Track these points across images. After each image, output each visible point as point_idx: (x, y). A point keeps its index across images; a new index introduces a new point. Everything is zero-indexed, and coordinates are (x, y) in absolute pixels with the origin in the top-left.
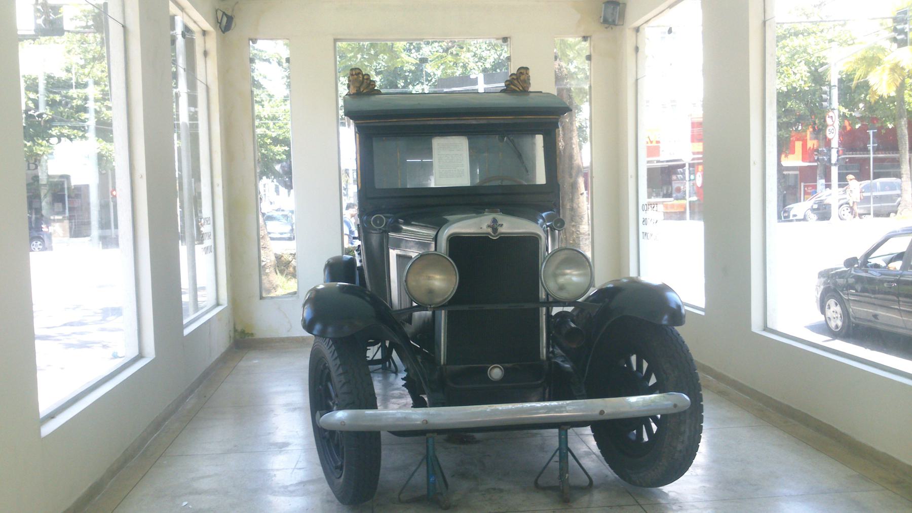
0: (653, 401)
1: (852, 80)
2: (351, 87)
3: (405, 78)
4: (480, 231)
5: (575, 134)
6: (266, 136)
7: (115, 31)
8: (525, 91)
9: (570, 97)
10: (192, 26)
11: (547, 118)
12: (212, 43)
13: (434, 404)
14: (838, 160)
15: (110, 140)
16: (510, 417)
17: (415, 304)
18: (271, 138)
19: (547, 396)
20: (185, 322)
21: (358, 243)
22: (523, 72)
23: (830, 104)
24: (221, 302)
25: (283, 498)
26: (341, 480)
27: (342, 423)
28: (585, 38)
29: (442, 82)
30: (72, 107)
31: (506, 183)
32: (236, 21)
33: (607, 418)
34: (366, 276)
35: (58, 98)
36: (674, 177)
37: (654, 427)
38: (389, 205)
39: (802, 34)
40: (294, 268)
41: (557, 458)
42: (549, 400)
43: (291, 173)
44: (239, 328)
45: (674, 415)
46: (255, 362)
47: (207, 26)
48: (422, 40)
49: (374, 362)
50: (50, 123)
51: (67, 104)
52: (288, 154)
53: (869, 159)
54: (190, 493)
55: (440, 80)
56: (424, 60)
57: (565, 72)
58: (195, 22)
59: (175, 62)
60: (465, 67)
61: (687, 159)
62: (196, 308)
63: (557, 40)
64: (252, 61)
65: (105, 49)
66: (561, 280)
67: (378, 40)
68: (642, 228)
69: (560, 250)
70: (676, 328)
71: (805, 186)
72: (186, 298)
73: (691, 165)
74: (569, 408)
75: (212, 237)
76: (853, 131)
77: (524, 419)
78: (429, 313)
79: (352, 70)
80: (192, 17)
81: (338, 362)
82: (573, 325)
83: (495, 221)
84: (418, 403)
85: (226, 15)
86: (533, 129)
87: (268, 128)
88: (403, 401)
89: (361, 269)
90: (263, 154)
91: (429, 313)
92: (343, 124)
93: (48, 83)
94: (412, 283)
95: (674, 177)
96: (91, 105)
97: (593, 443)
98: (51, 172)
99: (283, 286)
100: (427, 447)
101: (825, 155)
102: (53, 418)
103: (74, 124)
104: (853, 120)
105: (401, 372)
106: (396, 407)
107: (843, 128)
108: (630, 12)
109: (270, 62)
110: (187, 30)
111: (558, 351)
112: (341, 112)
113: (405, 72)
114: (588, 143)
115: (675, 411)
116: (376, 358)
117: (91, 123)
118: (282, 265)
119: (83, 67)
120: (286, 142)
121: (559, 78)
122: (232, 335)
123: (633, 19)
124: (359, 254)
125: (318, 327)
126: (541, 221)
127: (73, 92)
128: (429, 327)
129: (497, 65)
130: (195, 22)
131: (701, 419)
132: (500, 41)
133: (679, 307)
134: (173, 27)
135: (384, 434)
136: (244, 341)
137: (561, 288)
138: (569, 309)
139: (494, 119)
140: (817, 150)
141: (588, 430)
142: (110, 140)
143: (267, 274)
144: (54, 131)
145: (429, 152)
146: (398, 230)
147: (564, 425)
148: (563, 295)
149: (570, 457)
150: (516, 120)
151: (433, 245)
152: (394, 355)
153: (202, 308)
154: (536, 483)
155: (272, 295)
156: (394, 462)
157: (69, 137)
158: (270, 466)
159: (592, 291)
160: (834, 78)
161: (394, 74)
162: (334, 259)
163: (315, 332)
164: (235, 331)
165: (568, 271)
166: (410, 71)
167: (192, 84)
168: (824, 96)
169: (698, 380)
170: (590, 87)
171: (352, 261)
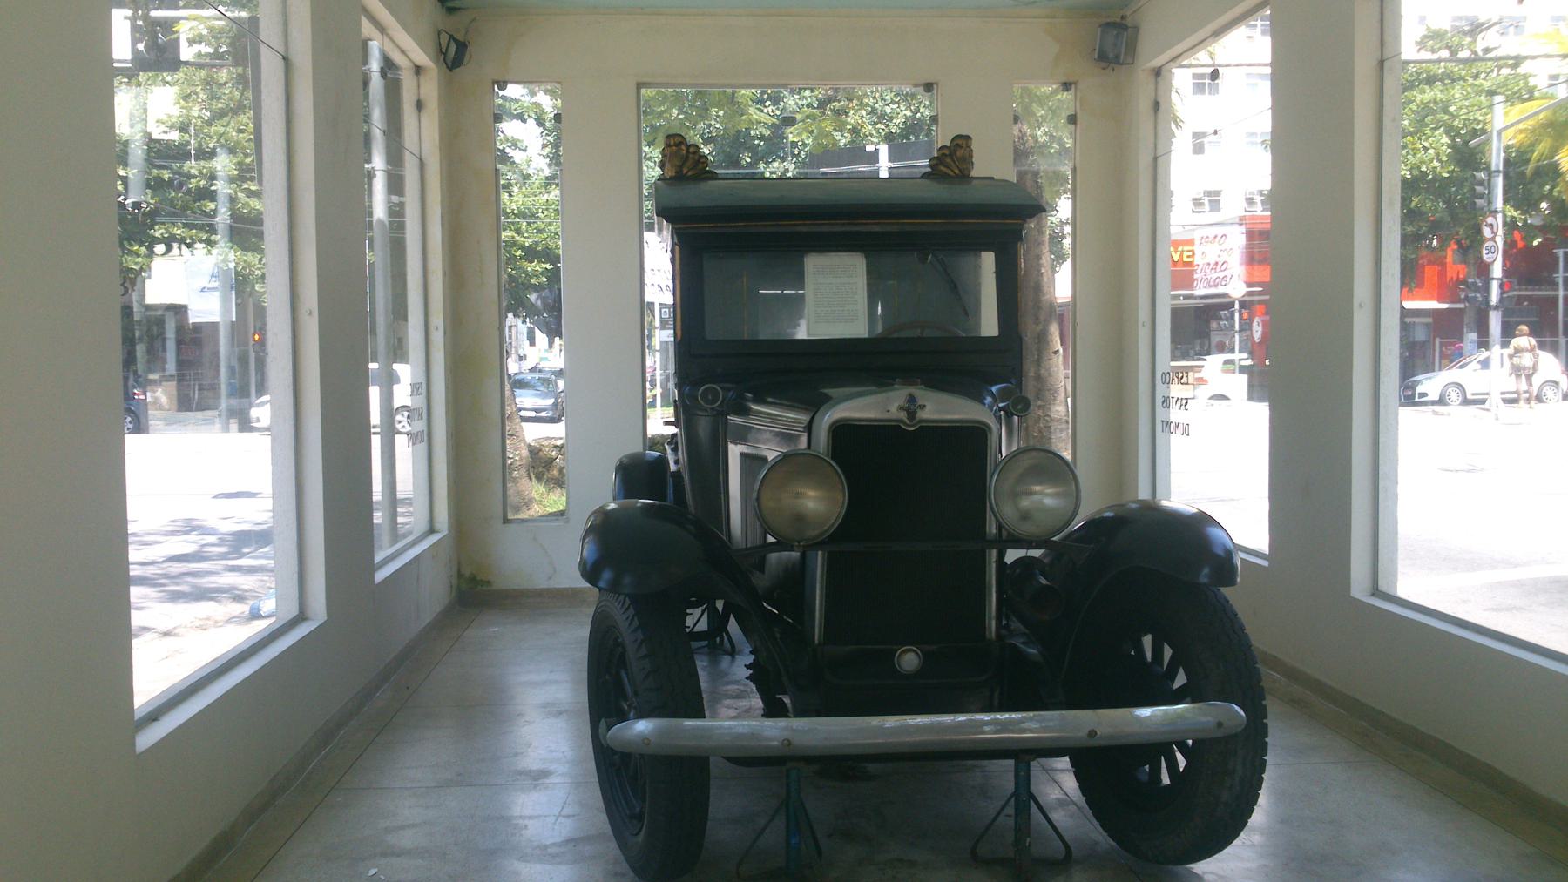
0: (1180, 716)
1: (1528, 161)
2: (668, 165)
3: (753, 150)
4: (886, 416)
5: (1046, 249)
6: (514, 243)
7: (271, 67)
8: (964, 177)
9: (1038, 187)
10: (397, 58)
11: (1005, 223)
12: (431, 88)
13: (801, 713)
14: (1501, 300)
15: (258, 249)
16: (925, 738)
17: (771, 539)
18: (523, 248)
19: (996, 702)
20: (378, 558)
21: (672, 430)
22: (961, 144)
23: (1490, 202)
24: (438, 526)
25: (538, 867)
26: (640, 838)
27: (645, 740)
28: (1066, 86)
29: (817, 159)
30: (189, 191)
31: (928, 333)
32: (471, 49)
33: (1103, 743)
34: (688, 488)
35: (166, 175)
36: (1214, 325)
37: (1182, 762)
38: (725, 367)
39: (1442, 80)
40: (561, 470)
41: (1010, 810)
42: (1001, 709)
43: (560, 310)
44: (467, 572)
45: (1217, 741)
46: (495, 631)
47: (422, 58)
48: (785, 86)
49: (699, 636)
50: (153, 217)
51: (181, 185)
52: (554, 276)
53: (1556, 298)
54: (384, 855)
55: (810, 155)
56: (789, 121)
57: (1031, 142)
58: (403, 52)
59: (367, 119)
60: (855, 131)
61: (1237, 289)
62: (395, 536)
63: (1017, 89)
64: (498, 118)
65: (249, 94)
66: (1025, 503)
67: (712, 85)
68: (1160, 413)
69: (1021, 452)
70: (1224, 590)
71: (1442, 345)
72: (378, 517)
73: (1243, 305)
74: (1029, 725)
75: (424, 415)
76: (1529, 249)
77: (961, 741)
78: (795, 555)
79: (669, 137)
80: (396, 41)
81: (640, 635)
82: (1044, 581)
83: (912, 399)
84: (773, 710)
85: (456, 41)
86: (977, 243)
87: (518, 231)
88: (744, 703)
89: (677, 476)
90: (510, 276)
91: (795, 555)
92: (650, 228)
93: (150, 150)
94: (768, 503)
95: (1214, 325)
96: (221, 187)
97: (1070, 783)
98: (150, 299)
99: (545, 500)
100: (788, 785)
101: (1477, 290)
102: (155, 720)
103: (191, 220)
104: (1530, 231)
105: (741, 652)
106: (735, 716)
107: (1509, 244)
108: (1145, 44)
109: (524, 121)
110: (388, 66)
111: (1016, 625)
112: (648, 205)
113: (754, 138)
114: (1069, 261)
115: (1219, 734)
116: (699, 628)
117: (223, 217)
118: (541, 464)
119: (209, 123)
120: (549, 255)
121: (1020, 154)
122: (455, 581)
123: (1148, 59)
124: (675, 450)
125: (607, 575)
126: (989, 400)
127: (192, 166)
128: (796, 578)
129: (911, 127)
130: (403, 52)
131: (1263, 749)
132: (921, 89)
133: (1229, 555)
134: (365, 60)
135: (717, 766)
136: (476, 594)
137: (1025, 516)
138: (1036, 553)
139: (908, 224)
140: (1464, 282)
141: (1064, 763)
142: (258, 249)
143: (515, 480)
144: (158, 232)
145: (799, 279)
146: (744, 411)
147: (1025, 754)
148: (1026, 529)
149: (1034, 809)
150: (950, 224)
151: (804, 439)
152: (733, 626)
153: (405, 536)
154: (973, 853)
155: (522, 516)
156: (729, 808)
157: (182, 241)
158: (516, 811)
159: (1077, 524)
160: (1496, 160)
161: (738, 141)
162: (627, 456)
163: (602, 584)
164: (460, 575)
165: (1038, 488)
166: (762, 138)
167: (395, 158)
168: (1479, 189)
169: (1259, 680)
170: (1074, 170)
171: (662, 461)
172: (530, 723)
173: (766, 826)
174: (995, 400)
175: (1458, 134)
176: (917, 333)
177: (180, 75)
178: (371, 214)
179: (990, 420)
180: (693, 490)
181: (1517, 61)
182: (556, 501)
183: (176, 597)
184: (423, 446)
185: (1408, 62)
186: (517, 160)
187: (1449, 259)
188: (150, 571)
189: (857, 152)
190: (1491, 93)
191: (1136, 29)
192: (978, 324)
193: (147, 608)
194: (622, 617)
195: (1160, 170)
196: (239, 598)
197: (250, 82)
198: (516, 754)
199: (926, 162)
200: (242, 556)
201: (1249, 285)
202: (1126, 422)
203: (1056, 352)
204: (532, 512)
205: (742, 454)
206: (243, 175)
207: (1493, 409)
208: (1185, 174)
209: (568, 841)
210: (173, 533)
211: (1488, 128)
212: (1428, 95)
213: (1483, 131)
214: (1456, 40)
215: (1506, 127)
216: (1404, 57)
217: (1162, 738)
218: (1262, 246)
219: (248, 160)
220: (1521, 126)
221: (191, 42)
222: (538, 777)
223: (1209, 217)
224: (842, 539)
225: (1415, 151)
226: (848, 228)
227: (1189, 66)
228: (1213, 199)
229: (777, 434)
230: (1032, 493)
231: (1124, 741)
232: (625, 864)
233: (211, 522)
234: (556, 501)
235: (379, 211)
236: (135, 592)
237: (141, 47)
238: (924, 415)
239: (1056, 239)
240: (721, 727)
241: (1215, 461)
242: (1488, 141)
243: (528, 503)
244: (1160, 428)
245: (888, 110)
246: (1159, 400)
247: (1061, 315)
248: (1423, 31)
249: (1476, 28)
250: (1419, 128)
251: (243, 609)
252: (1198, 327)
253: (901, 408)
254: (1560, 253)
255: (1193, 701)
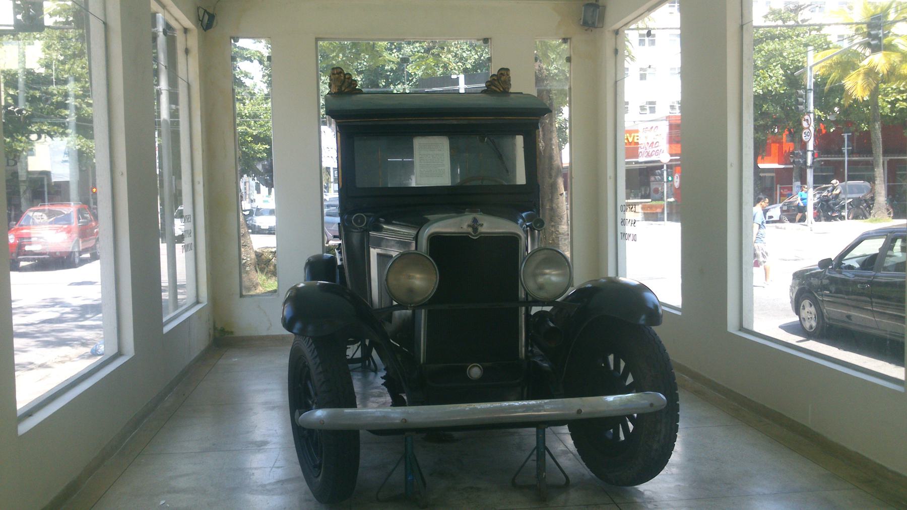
0: (629, 400)
3: (387, 77)
4: (460, 230)
5: (555, 135)
7: (96, 28)
8: (506, 92)
10: (173, 23)
11: (529, 119)
12: (193, 41)
14: (813, 163)
15: (91, 137)
17: (395, 303)
18: (252, 136)
20: (164, 320)
22: (504, 73)
23: (806, 107)
24: (201, 299)
25: (260, 497)
26: (319, 479)
27: (321, 421)
28: (565, 40)
29: (422, 82)
30: (52, 104)
31: (485, 183)
34: (347, 274)
35: (38, 94)
36: (652, 178)
37: (631, 426)
38: (369, 203)
39: (779, 38)
40: (275, 266)
41: (534, 457)
42: (528, 399)
44: (219, 327)
46: (235, 359)
47: (188, 24)
48: (403, 40)
49: (353, 361)
50: (30, 119)
51: (47, 100)
52: (269, 152)
54: (169, 492)
57: (546, 73)
58: (176, 20)
59: (156, 59)
60: (445, 67)
61: (665, 158)
62: (176, 305)
64: (234, 59)
65: (85, 45)
66: (541, 280)
69: (539, 250)
70: (654, 328)
72: (165, 296)
74: (546, 407)
75: (192, 234)
76: (828, 134)
77: (499, 417)
78: (409, 312)
80: (172, 15)
82: (552, 325)
83: (475, 220)
84: (397, 402)
85: (208, 13)
86: (513, 130)
87: (249, 126)
88: (382, 400)
89: (341, 267)
90: (244, 152)
91: (409, 312)
92: (325, 124)
95: (652, 178)
96: (71, 101)
97: (570, 442)
99: (266, 284)
101: (801, 157)
103: (54, 120)
104: (829, 123)
105: (380, 371)
106: (375, 407)
107: (818, 131)
109: (252, 61)
110: (168, 28)
111: (536, 350)
112: (323, 111)
113: (387, 71)
115: (651, 410)
117: (72, 119)
118: (263, 263)
119: (63, 63)
120: (266, 140)
121: (539, 79)
122: (212, 332)
123: (611, 24)
124: (340, 253)
125: (298, 326)
126: (521, 221)
127: (53, 88)
128: (410, 325)
129: (478, 65)
130: (176, 20)
133: (656, 307)
134: (154, 24)
136: (224, 339)
137: (541, 287)
138: (548, 309)
139: (473, 120)
140: (793, 153)
141: (565, 429)
142: (91, 137)
143: (247, 272)
144: (34, 128)
145: (410, 152)
146: (379, 229)
147: (542, 424)
148: (542, 295)
149: (548, 456)
150: (497, 121)
151: (414, 244)
152: (374, 353)
153: (182, 306)
155: (252, 293)
156: (372, 459)
159: (571, 291)
160: (810, 83)
161: (375, 73)
162: (314, 257)
163: (295, 331)
164: (215, 328)
165: (547, 271)
166: (392, 70)
167: (173, 82)
169: (674, 379)
171: (333, 259)
172: (255, 414)
173: (393, 470)
174: (524, 221)
175: (789, 69)
176: (478, 183)
177: (44, 34)
178: (159, 117)
179: (523, 235)
180: (350, 275)
181: (820, 27)
182: (272, 284)
183: (47, 344)
184: (191, 253)
185: (758, 28)
186: (247, 84)
187: (784, 140)
188: (23, 330)
189: (447, 79)
190: (806, 45)
191: (604, 7)
192: (515, 176)
193: (25, 352)
194: (308, 350)
195: (619, 89)
196: (84, 343)
197: (85, 38)
198: (248, 432)
199: (484, 85)
200: (87, 319)
201: (671, 155)
202: (600, 235)
203: (561, 194)
204: (258, 291)
205: (378, 254)
206: (86, 93)
207: (809, 224)
208: (634, 91)
209: (278, 482)
210: (45, 306)
211: (805, 65)
212: (771, 46)
213: (803, 67)
214: (786, 15)
215: (815, 64)
216: (755, 23)
217: (619, 413)
218: (678, 133)
219: (87, 85)
220: (823, 64)
221: (51, 15)
222: (261, 445)
223: (649, 116)
224: (435, 303)
225: (764, 79)
226: (439, 122)
227: (638, 29)
228: (652, 106)
229: (398, 242)
230: (545, 274)
231: (596, 416)
232: (311, 495)
233: (68, 299)
234: (272, 284)
235: (165, 114)
236: (18, 343)
237: (19, 17)
238: (483, 230)
239: (561, 130)
240: (368, 413)
241: (651, 258)
242: (804, 73)
243: (255, 286)
244: (620, 237)
245: (465, 55)
246: (619, 221)
247: (567, 176)
248: (766, 11)
249: (797, 9)
250: (766, 65)
251: (88, 350)
252: (642, 179)
253: (469, 226)
254: (846, 136)
255: (637, 392)
